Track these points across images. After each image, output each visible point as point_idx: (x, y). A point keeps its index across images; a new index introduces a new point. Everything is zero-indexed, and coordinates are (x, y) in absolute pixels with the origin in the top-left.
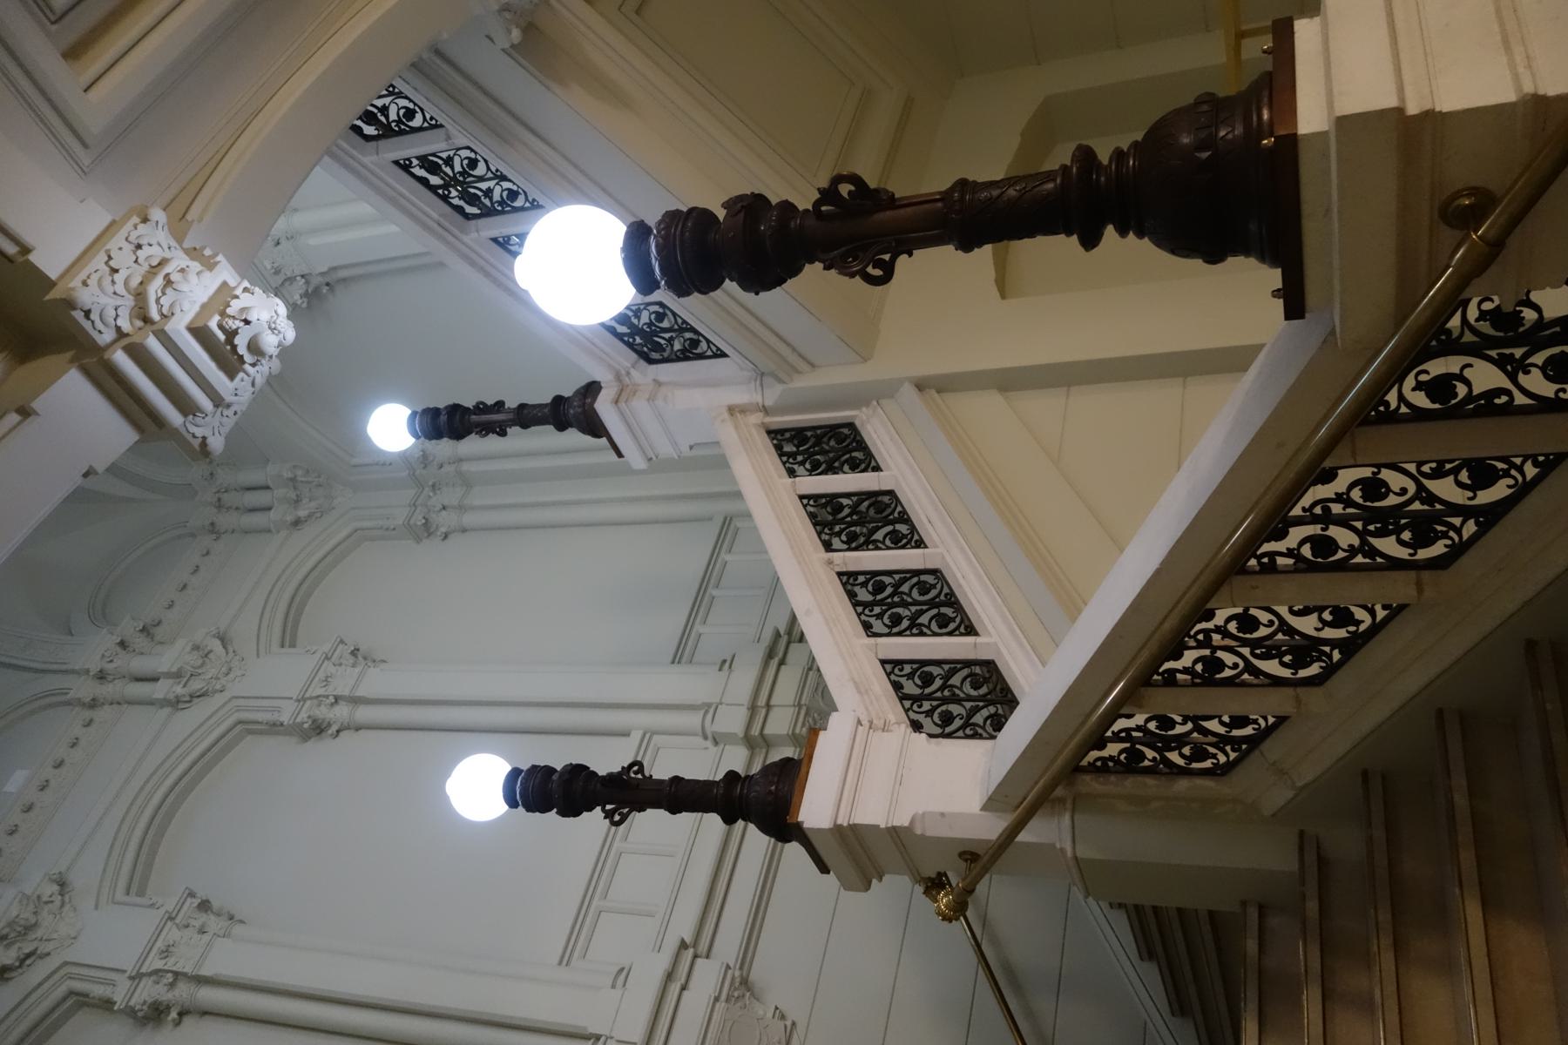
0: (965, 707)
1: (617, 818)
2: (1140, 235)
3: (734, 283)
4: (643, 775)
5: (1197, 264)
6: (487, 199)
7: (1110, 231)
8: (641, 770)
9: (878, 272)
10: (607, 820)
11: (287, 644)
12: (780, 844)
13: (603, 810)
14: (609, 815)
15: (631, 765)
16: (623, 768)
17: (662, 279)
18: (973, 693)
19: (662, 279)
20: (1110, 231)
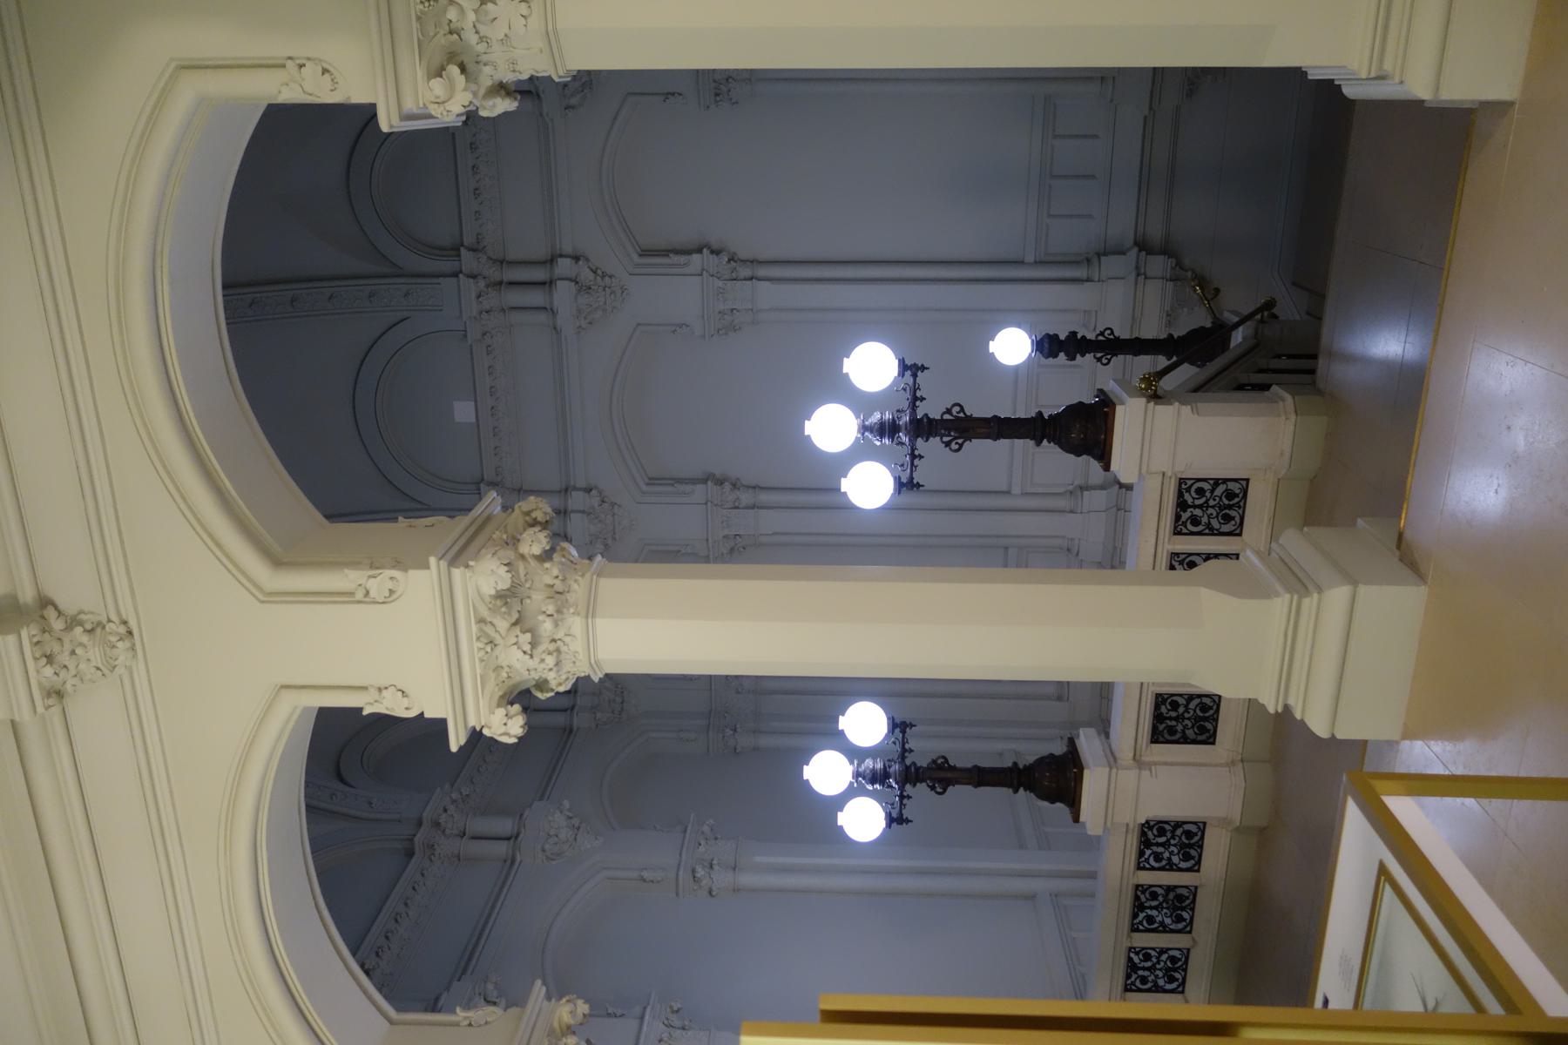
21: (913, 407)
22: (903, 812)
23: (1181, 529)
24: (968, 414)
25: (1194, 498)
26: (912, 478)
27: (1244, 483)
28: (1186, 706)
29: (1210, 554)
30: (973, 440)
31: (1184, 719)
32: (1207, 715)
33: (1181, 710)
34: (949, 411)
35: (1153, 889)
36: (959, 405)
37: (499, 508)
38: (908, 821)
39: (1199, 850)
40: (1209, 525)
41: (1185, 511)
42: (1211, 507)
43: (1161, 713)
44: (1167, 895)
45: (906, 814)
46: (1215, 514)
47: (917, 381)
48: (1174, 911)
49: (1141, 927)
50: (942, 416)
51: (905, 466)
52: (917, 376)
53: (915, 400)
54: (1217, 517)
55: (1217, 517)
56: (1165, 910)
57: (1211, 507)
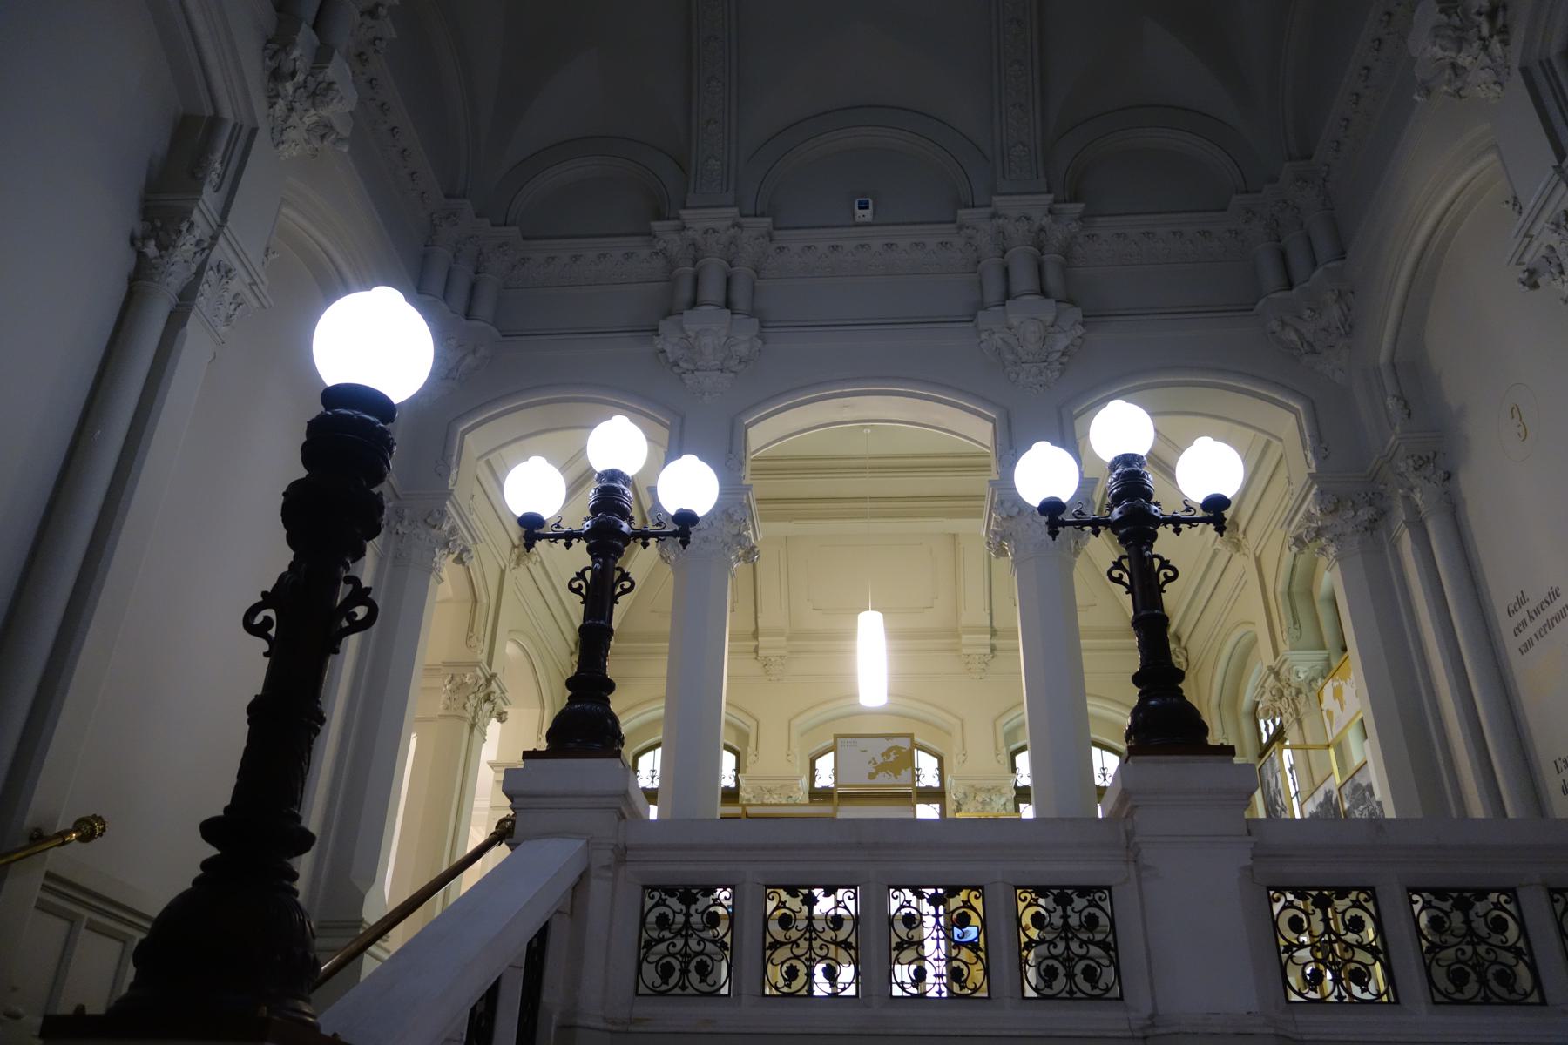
0: (1517, 941)
1: (1116, 574)
2: (196, 882)
3: (190, 886)
4: (1164, 583)
5: (302, 438)
6: (1086, 939)
7: (211, 851)
8: (1169, 579)
9: (259, 619)
10: (1112, 565)
11: (763, 506)
12: (148, 925)
13: (1122, 557)
14: (1118, 565)
15: (1174, 569)
16: (1168, 561)
17: (333, 413)
18: (1490, 975)
19: (333, 413)
20: (211, 851)
21: (1166, 521)
22: (544, 541)
23: (1417, 902)
24: (1165, 588)
25: (1343, 913)
26: (1064, 524)
27: (1116, 992)
28: (1091, 942)
29: (1116, 950)
30: (1130, 595)
31: (1067, 940)
32: (1493, 984)
33: (1351, 937)
34: (1165, 564)
35: (705, 921)
36: (1109, 573)
37: (1498, 45)
38: (1053, 533)
39: (1478, 999)
40: (776, 945)
41: (681, 900)
42: (811, 945)
43: (1473, 904)
44: (1508, 949)
45: (541, 545)
46: (797, 952)
47: (668, 538)
48: (1473, 967)
49: (1277, 908)
50: (1157, 556)
51: (1080, 516)
52: (675, 537)
53: (1176, 522)
54: (1460, 962)
55: (1460, 962)
56: (1469, 950)
57: (811, 945)
